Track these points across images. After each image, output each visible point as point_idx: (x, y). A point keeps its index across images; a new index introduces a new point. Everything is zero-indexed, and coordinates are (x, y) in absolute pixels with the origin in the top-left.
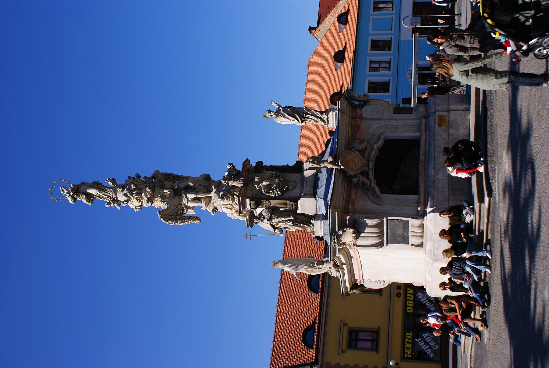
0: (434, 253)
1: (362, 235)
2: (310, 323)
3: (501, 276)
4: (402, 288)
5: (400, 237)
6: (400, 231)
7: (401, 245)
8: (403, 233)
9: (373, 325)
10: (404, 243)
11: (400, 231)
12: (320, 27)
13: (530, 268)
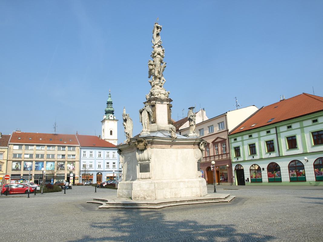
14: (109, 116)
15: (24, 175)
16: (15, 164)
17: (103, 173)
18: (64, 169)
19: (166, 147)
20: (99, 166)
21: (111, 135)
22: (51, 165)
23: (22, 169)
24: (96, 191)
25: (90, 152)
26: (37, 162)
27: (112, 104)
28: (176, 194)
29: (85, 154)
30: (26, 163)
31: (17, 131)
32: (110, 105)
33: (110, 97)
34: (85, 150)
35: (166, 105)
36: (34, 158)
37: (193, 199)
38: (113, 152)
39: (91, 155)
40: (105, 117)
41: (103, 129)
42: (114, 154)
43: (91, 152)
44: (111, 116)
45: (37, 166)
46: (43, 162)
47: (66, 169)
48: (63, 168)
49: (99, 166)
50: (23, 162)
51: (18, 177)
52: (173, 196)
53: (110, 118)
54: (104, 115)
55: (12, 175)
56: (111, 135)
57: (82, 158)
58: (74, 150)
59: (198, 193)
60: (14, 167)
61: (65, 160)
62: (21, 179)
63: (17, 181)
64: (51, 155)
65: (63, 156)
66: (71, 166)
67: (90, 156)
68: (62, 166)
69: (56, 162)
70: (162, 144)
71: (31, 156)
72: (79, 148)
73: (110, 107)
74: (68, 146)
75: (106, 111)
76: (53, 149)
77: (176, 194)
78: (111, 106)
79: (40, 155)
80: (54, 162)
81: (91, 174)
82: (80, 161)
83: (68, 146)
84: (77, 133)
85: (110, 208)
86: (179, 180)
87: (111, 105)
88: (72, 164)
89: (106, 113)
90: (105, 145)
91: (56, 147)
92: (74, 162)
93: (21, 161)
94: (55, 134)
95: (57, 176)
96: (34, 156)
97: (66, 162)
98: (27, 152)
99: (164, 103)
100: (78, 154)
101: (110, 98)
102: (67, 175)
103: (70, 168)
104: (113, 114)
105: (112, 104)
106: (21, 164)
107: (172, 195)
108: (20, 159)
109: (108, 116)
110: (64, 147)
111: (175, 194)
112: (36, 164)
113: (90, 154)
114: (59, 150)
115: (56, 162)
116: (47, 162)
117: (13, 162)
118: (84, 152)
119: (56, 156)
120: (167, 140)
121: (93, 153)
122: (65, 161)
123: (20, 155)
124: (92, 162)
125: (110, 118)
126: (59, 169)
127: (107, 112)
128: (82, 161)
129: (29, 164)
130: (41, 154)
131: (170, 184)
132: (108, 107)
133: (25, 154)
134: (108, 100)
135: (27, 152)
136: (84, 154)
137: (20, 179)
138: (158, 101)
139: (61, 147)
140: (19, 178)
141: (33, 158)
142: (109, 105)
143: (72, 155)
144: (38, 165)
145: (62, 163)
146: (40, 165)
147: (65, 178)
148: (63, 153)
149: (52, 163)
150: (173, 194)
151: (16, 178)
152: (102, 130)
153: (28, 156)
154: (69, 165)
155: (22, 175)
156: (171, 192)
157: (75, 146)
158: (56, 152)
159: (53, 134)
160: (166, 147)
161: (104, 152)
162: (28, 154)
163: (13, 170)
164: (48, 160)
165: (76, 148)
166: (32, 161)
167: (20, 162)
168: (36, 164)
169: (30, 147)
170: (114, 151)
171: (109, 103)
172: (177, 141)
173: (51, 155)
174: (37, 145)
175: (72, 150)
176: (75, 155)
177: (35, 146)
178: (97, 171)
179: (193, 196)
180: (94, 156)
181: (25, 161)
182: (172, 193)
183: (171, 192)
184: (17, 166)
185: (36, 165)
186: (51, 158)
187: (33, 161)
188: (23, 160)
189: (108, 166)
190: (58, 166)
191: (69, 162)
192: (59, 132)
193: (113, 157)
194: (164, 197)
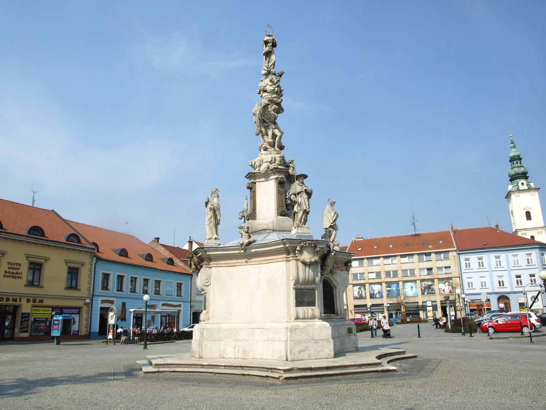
0: (297, 329)
1: (307, 269)
2: (46, 235)
3: (55, 378)
4: (7, 303)
5: (302, 299)
6: (306, 300)
7: (295, 301)
8: (305, 302)
9: (45, 282)
10: (296, 303)
11: (306, 300)
12: (159, 246)
13: (11, 394)
14: (518, 183)
15: (373, 305)
16: (356, 288)
17: (511, 296)
18: (433, 292)
19: (237, 263)
20: (501, 284)
21: (527, 220)
22: (412, 287)
23: (368, 296)
24: (419, 334)
25: (479, 259)
26: (389, 284)
27: (520, 159)
28: (245, 352)
29: (469, 263)
30: (373, 286)
31: (357, 238)
32: (517, 163)
33: (515, 147)
34: (467, 256)
35: (273, 180)
36: (384, 279)
37: (234, 365)
38: (528, 254)
39: (481, 265)
40: (510, 187)
41: (512, 211)
42: (529, 258)
43: (480, 259)
44: (523, 184)
45: (390, 290)
46: (397, 283)
47: (437, 292)
48: (432, 290)
49: (501, 284)
50: (367, 285)
51: (364, 308)
52: (240, 355)
53: (521, 188)
54: (508, 185)
55: (355, 306)
56: (527, 220)
57: (463, 271)
58: (446, 258)
59: (282, 354)
60: (356, 294)
61: (416, 279)
62: (369, 312)
63: (364, 315)
64: (408, 271)
65: (430, 269)
66: (446, 288)
67: (480, 266)
68: (429, 287)
69: (418, 282)
70: (230, 259)
71: (378, 274)
72: (454, 253)
73: (518, 167)
74: (436, 253)
75: (510, 176)
76: (411, 260)
77: (245, 352)
78: (519, 165)
79: (391, 272)
80: (415, 281)
81: (420, 304)
82: (460, 277)
83: (436, 253)
84: (452, 228)
85: (166, 371)
86: (254, 326)
87: (519, 161)
88: (447, 283)
89: (511, 180)
90: (513, 242)
91: (416, 256)
92: (451, 278)
93: (363, 284)
94: (416, 235)
95: (423, 306)
96: (383, 275)
97: (436, 281)
98: (371, 269)
99: (271, 177)
100: (455, 265)
101: (514, 150)
102: (441, 304)
103: (444, 290)
104: (526, 178)
105: (520, 159)
106: (365, 289)
107: (238, 352)
108: (362, 282)
109: (515, 185)
110: (428, 254)
111: (243, 350)
112: (387, 287)
113: (479, 263)
114: (371, 265)
115: (418, 282)
116: (404, 282)
117: (353, 286)
118: (466, 260)
119: (417, 272)
120: (276, 245)
121: (485, 260)
122: (434, 279)
123: (362, 274)
124: (471, 278)
125: (521, 188)
126: (426, 293)
127: (513, 178)
128: (464, 276)
129: (377, 288)
130: (393, 271)
131: (236, 332)
132: (513, 168)
133: (369, 273)
134: (511, 154)
135: (371, 269)
136: (466, 264)
137: (367, 312)
138: (259, 178)
139: (424, 256)
140: (366, 311)
141: (381, 278)
142: (515, 162)
143: (445, 267)
144: (391, 289)
145: (430, 283)
146: (394, 288)
147: (438, 308)
148: (429, 265)
149: (413, 284)
150: (241, 351)
151: (361, 311)
152: (508, 214)
153: (374, 276)
154: (442, 286)
155: (368, 306)
156: (235, 347)
157: (448, 252)
158: (415, 264)
159: (413, 235)
160: (237, 263)
161: (507, 257)
162: (374, 273)
163: (356, 298)
164: (405, 279)
165: (450, 254)
166: (380, 283)
167: (363, 285)
168: (387, 287)
169: (375, 262)
170: (466, 257)
171: (515, 159)
172: (253, 250)
173: (408, 271)
174: (385, 257)
175: (443, 258)
176: (449, 267)
177: (382, 259)
178: (496, 293)
179: (276, 358)
180: (487, 264)
181: (370, 284)
182: (238, 350)
183: (235, 347)
184: (360, 292)
185: (388, 289)
186: (409, 275)
187: (382, 283)
188: (419, 279)
189: (519, 283)
190: (423, 289)
191: (439, 279)
192: (422, 229)
193: (529, 263)
194: (220, 355)
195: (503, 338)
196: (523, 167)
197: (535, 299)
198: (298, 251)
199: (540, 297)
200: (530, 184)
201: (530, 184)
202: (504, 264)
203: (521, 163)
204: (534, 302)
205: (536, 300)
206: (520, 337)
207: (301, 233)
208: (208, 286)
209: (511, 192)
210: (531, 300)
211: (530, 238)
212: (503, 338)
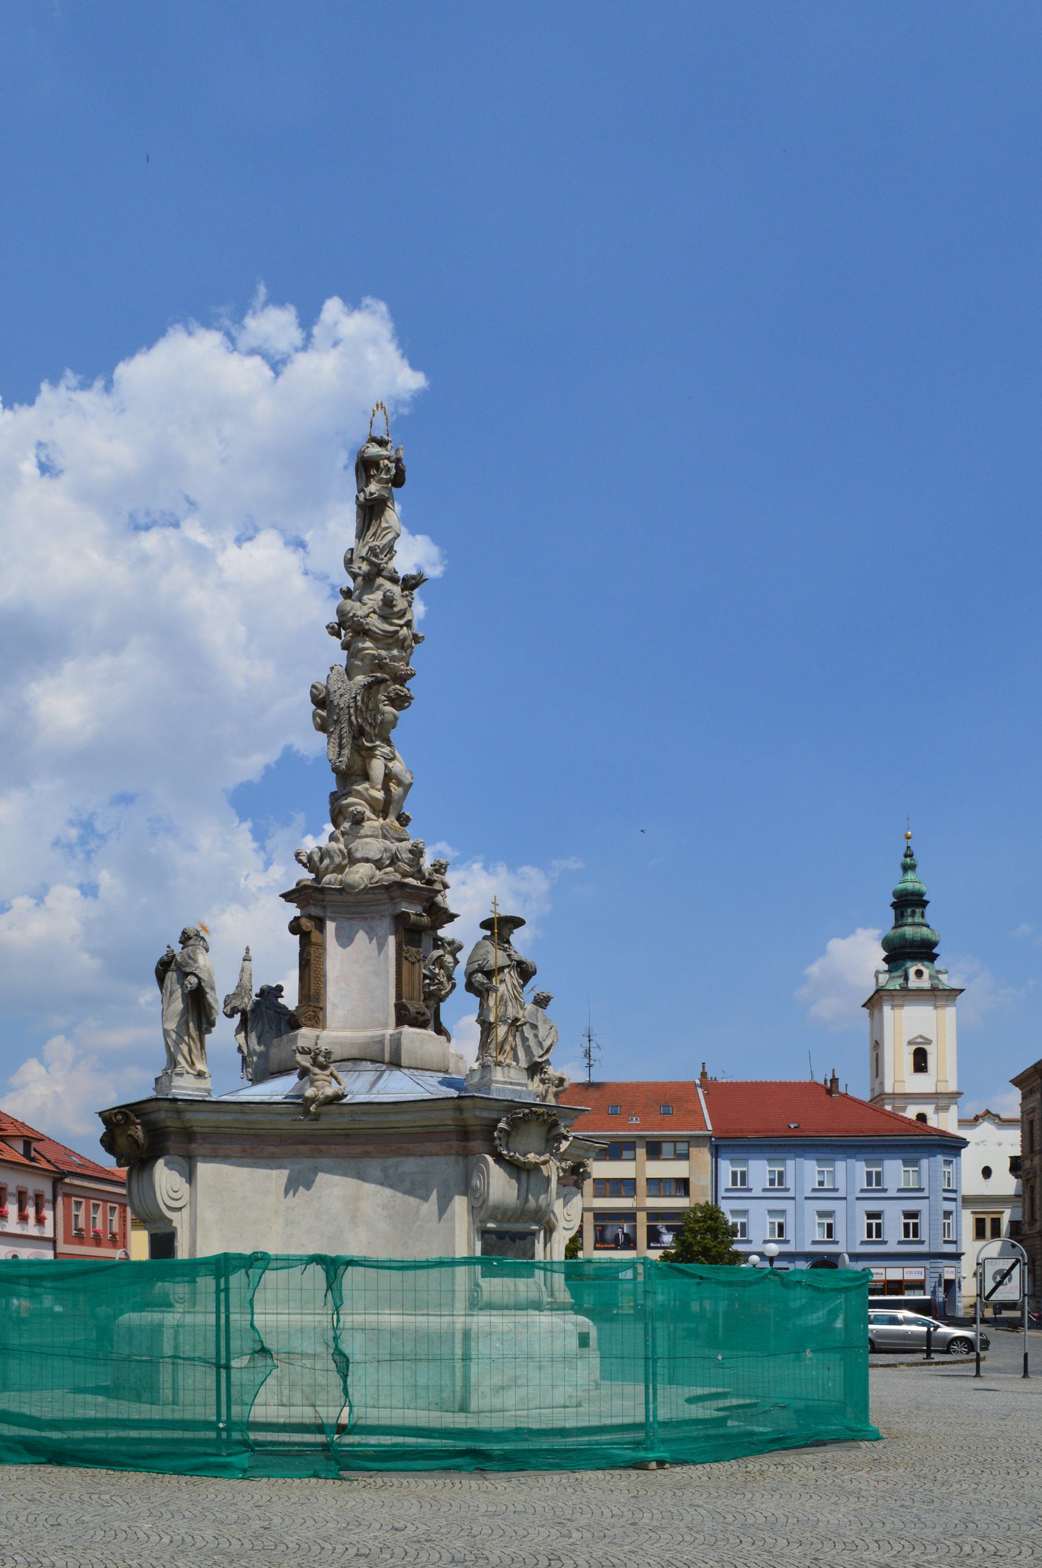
53: (914, 983)
57: (722, 1193)
84: (704, 1074)
105: (924, 904)
159: (582, 1084)
195: (882, 1366)
196: (928, 926)
197: (1004, 1277)
198: (502, 1130)
199: (1016, 1273)
200: (940, 976)
201: (940, 976)
202: (790, 1182)
203: (923, 915)
204: (999, 1284)
205: (1006, 1280)
206: (922, 1364)
207: (505, 1083)
208: (180, 1209)
209: (882, 993)
210: (994, 1278)
211: (914, 1118)
212: (882, 1366)
